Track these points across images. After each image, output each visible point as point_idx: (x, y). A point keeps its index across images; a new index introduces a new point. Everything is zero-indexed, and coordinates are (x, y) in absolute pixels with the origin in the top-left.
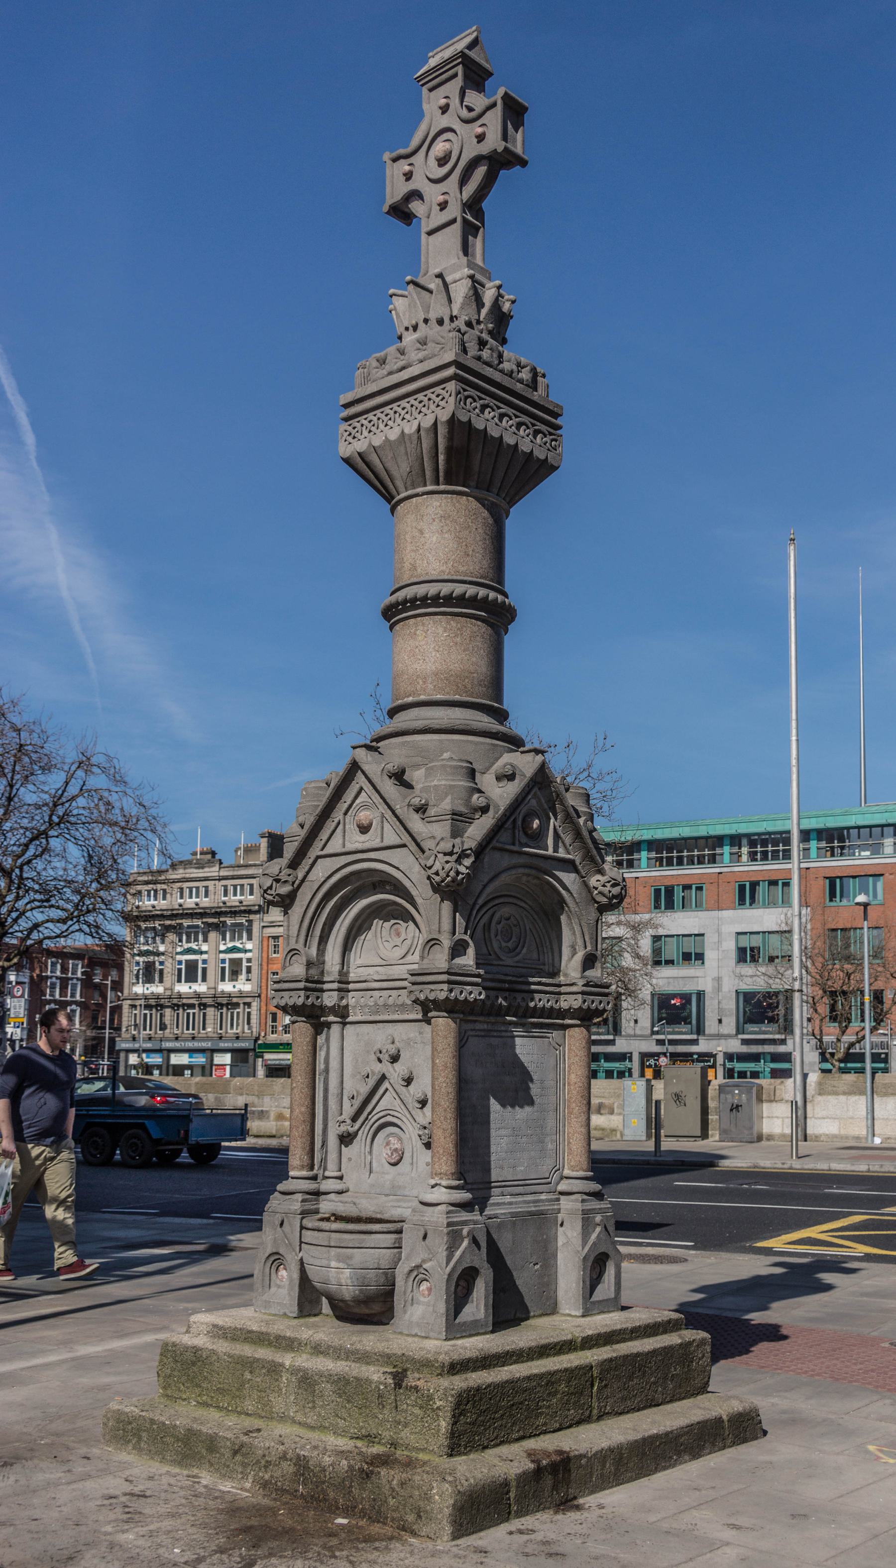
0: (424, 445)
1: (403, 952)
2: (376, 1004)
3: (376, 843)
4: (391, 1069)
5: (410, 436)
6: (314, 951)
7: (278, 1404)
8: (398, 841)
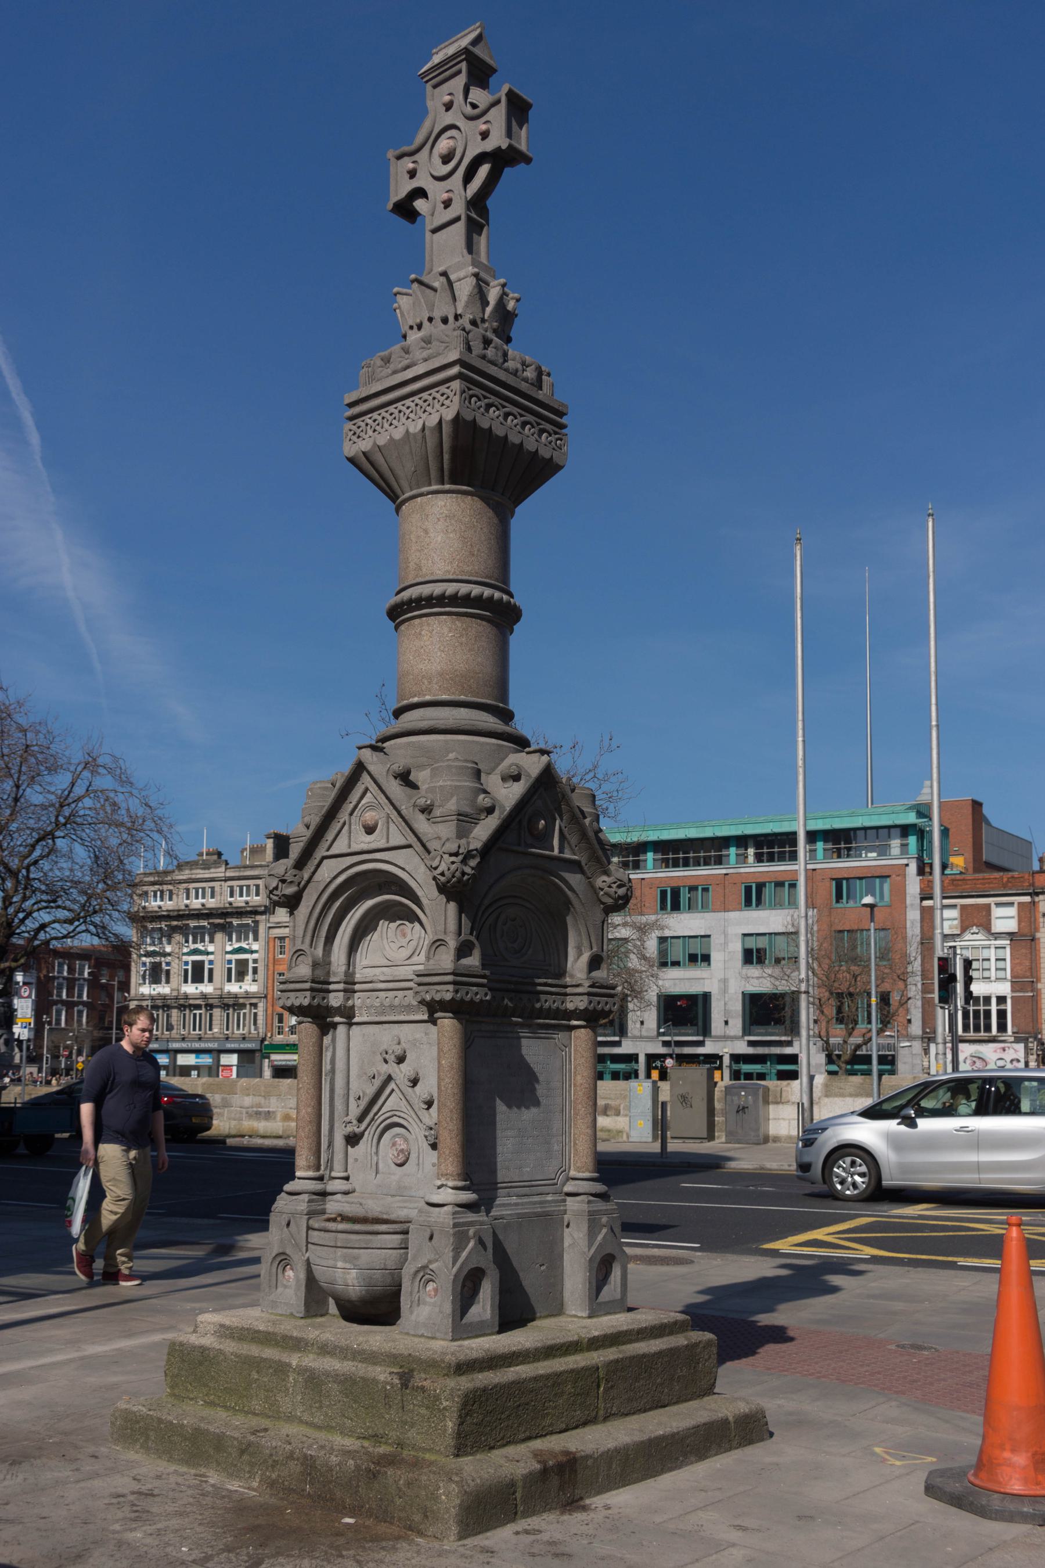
0: (429, 444)
1: (409, 953)
2: (382, 1005)
3: (382, 844)
4: (397, 1070)
5: (414, 435)
6: (319, 951)
7: (285, 1404)
8: (402, 841)
